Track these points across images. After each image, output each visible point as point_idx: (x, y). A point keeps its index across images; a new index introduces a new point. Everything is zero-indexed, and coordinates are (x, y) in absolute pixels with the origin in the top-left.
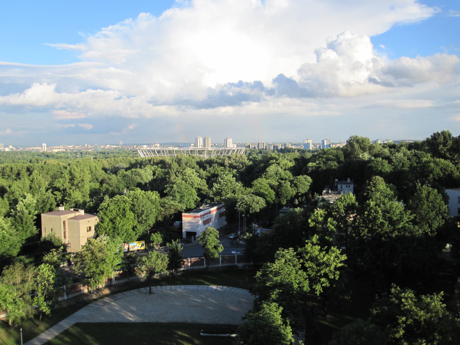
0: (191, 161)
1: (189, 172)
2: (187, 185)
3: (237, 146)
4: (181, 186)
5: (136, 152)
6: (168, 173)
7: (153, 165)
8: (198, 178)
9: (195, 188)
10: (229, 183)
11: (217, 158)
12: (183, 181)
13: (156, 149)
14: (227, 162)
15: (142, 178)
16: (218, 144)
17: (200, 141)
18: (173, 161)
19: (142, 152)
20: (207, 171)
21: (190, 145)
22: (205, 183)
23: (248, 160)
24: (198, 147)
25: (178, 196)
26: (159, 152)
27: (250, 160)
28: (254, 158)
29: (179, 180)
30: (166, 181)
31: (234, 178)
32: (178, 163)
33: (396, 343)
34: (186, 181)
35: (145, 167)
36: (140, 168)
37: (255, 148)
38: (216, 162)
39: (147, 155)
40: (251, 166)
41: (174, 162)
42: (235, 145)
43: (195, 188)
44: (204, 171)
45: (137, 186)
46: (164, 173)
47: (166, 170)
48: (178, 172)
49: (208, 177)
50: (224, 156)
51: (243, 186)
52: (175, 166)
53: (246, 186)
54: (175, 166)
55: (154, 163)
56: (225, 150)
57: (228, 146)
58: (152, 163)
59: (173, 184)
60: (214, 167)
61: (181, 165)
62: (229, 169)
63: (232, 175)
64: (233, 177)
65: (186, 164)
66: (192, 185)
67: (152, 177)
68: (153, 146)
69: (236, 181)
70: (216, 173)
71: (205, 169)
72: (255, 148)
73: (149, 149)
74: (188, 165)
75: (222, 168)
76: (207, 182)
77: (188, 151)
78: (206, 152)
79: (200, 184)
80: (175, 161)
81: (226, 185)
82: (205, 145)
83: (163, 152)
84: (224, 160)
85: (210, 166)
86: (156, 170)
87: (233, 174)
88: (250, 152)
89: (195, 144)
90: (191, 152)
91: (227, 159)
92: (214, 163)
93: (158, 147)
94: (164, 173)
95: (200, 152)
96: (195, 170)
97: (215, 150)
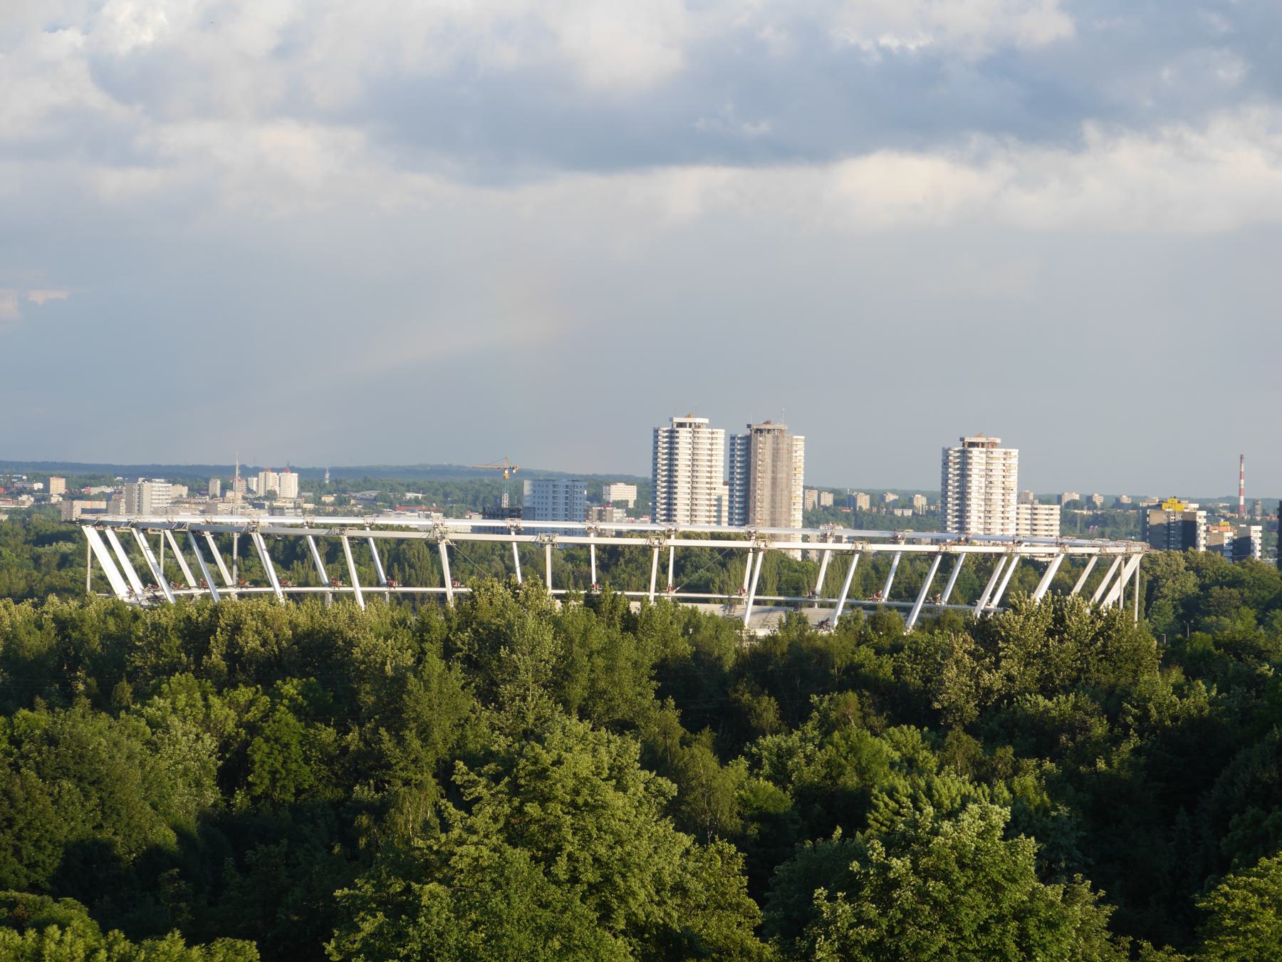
0: (609, 650)
1: (585, 764)
2: (554, 893)
3: (1069, 523)
4: (496, 902)
5: (67, 547)
6: (369, 765)
7: (224, 684)
8: (666, 827)
9: (636, 929)
10: (974, 896)
11: (861, 640)
12: (520, 856)
13: (265, 519)
14: (954, 684)
15: (108, 809)
16: (878, 498)
17: (704, 460)
18: (420, 658)
19: (129, 545)
20: (755, 763)
21: (597, 498)
22: (737, 884)
23: (1166, 664)
24: (682, 524)
25: (44, 569)
26: (289, 552)
27: (1197, 666)
28: (1236, 648)
29: (476, 842)
30: (350, 843)
31: (1029, 845)
32: (472, 664)
33: (1280, 667)
34: (547, 858)
35: (143, 696)
36: (104, 702)
37: (1242, 546)
38: (854, 678)
39: (174, 577)
40: (1195, 725)
41: (435, 663)
42: (1051, 517)
43: (636, 929)
44: (725, 755)
45: (60, 886)
46: (329, 760)
47: (352, 738)
48: (474, 762)
49: (762, 816)
50: (933, 621)
51: (1116, 926)
52: (442, 692)
53: (1140, 932)
54: (442, 692)
55: (234, 656)
56: (949, 560)
57: (975, 526)
58: (216, 658)
59: (424, 872)
60: (827, 727)
61: (506, 690)
62: (973, 746)
63: (1000, 815)
64: (1011, 830)
65: (557, 684)
66: (604, 894)
67: (211, 796)
68: (236, 495)
69: (1047, 875)
70: (851, 780)
71: (734, 737)
72: (1242, 546)
73: (189, 517)
74: (577, 692)
75: (910, 735)
76: (750, 870)
77: (574, 556)
78: (753, 571)
79: (680, 889)
80: (448, 652)
81: (946, 913)
82: (744, 510)
83: (333, 552)
84: (931, 659)
85: (794, 716)
86: (253, 729)
87: (1017, 803)
88: (1191, 583)
89: (647, 491)
90: (602, 567)
91: (963, 644)
92: (827, 684)
93: (282, 504)
94: (329, 760)
95: (704, 570)
96: (635, 748)
97: (842, 559)
